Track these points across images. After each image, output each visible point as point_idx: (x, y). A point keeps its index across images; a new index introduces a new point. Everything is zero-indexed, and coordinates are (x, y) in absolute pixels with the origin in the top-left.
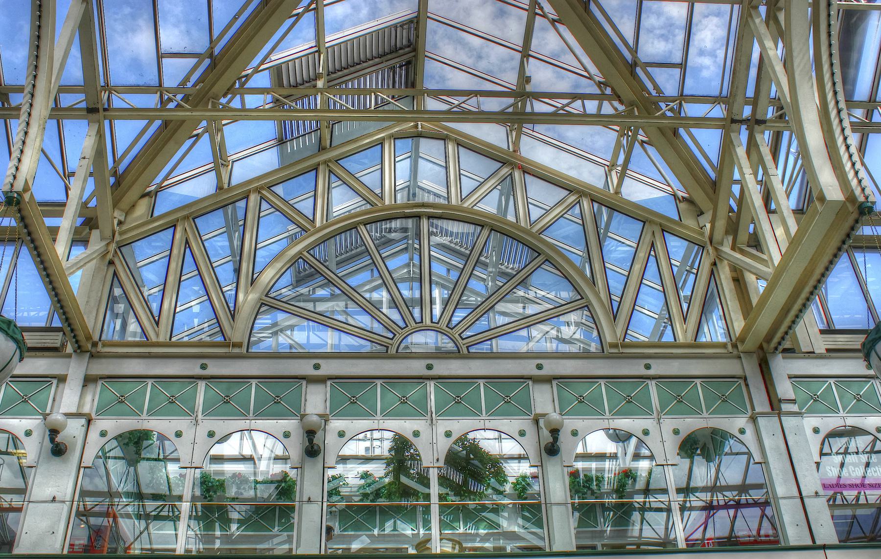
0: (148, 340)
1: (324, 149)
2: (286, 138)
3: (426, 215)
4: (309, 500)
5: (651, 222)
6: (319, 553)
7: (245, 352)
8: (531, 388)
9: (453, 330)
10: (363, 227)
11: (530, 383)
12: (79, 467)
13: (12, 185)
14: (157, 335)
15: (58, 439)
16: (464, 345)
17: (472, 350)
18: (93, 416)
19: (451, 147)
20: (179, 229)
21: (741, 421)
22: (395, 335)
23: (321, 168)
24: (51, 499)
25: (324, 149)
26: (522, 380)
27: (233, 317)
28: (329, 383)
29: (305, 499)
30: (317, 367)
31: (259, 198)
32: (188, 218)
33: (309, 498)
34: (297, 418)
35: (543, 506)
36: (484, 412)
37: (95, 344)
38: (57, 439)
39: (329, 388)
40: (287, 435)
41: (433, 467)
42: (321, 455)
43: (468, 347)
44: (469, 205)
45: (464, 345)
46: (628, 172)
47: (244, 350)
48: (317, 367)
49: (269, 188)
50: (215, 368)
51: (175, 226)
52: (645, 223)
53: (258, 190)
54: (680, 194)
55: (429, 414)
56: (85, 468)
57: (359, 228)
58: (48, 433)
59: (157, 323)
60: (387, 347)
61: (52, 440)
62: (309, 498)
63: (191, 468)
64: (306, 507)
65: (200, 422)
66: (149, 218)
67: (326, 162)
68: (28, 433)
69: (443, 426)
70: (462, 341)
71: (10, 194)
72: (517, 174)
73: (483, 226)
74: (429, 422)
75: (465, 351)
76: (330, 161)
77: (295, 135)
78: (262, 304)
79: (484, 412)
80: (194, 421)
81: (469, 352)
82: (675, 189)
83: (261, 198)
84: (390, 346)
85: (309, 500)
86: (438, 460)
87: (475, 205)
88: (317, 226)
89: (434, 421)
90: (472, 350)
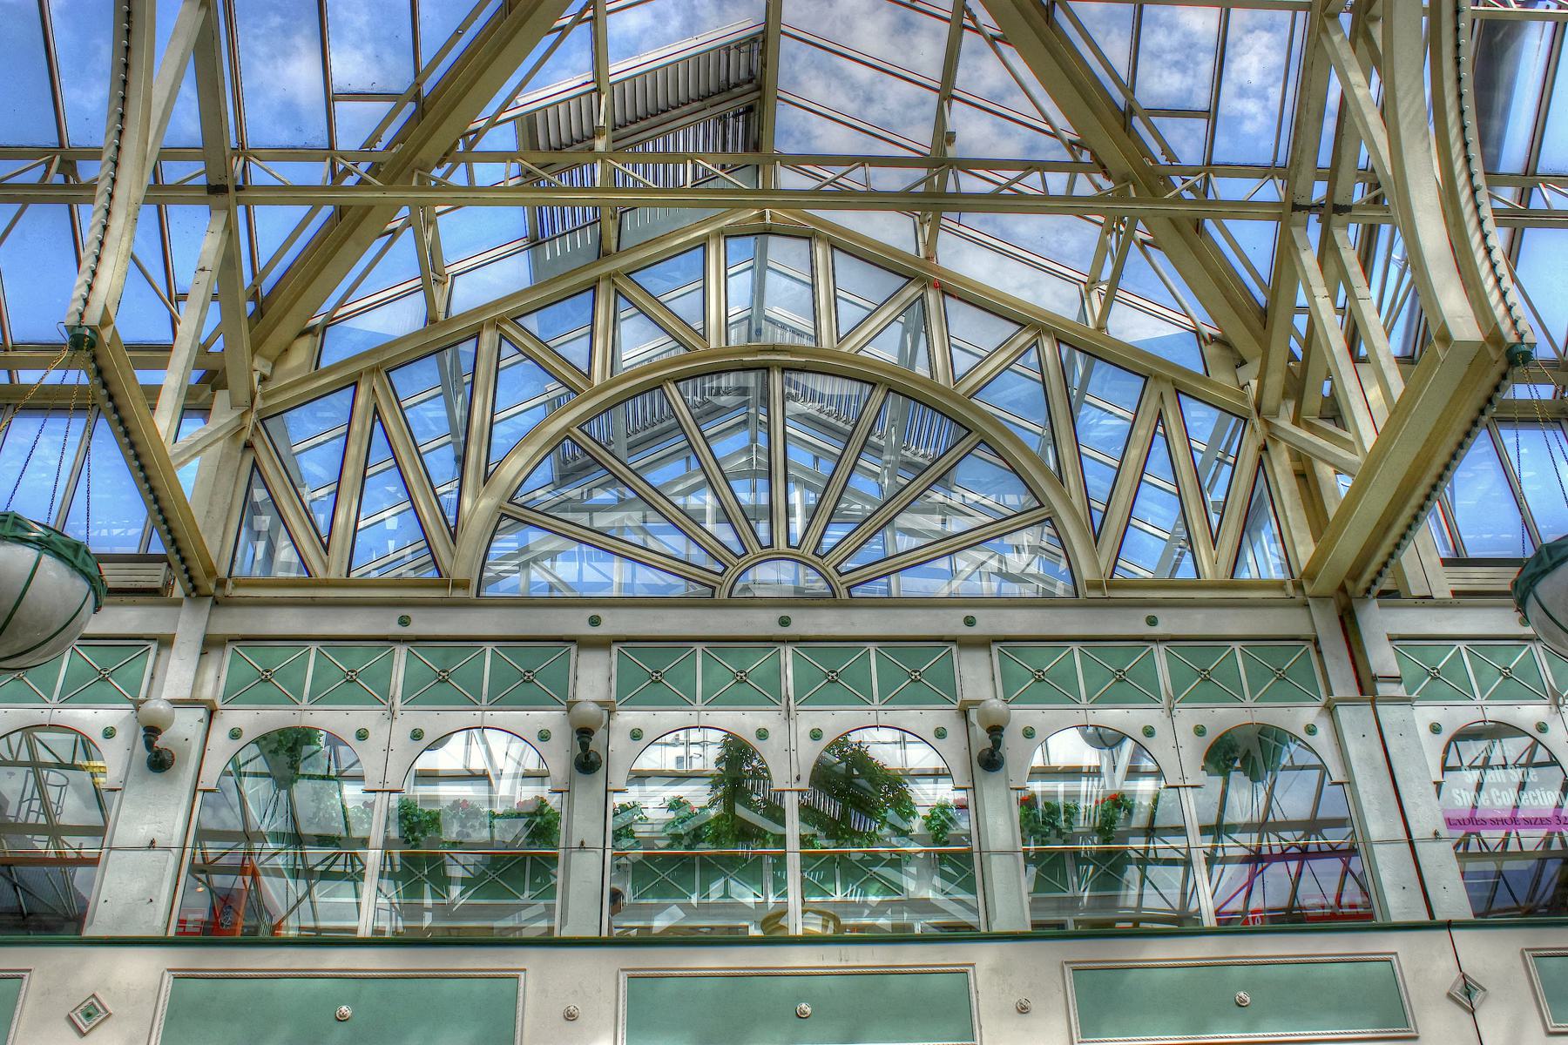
0: (310, 575)
1: (607, 254)
2: (543, 236)
3: (778, 367)
4: (582, 845)
5: (1158, 377)
6: (597, 935)
7: (474, 596)
8: (955, 656)
9: (825, 560)
10: (672, 387)
11: (954, 648)
12: (195, 791)
13: (82, 315)
14: (326, 568)
15: (160, 743)
16: (842, 584)
17: (857, 593)
18: (219, 704)
19: (820, 251)
20: (363, 389)
21: (1309, 713)
22: (726, 568)
23: (602, 286)
24: (148, 844)
25: (607, 254)
26: (940, 644)
27: (454, 537)
28: (615, 648)
29: (575, 843)
30: (595, 621)
31: (497, 337)
32: (378, 370)
33: (582, 843)
34: (561, 707)
35: (976, 856)
36: (876, 698)
37: (221, 584)
38: (157, 743)
39: (615, 658)
40: (544, 736)
41: (383, 791)
42: (602, 770)
43: (849, 589)
44: (852, 349)
45: (842, 584)
46: (1119, 293)
47: (472, 593)
48: (970, 622)
49: (514, 320)
50: (423, 624)
51: (356, 384)
52: (1147, 378)
53: (496, 324)
54: (1207, 330)
55: (784, 700)
56: (204, 791)
57: (665, 388)
58: (142, 733)
59: (326, 548)
60: (714, 588)
61: (149, 745)
62: (582, 843)
63: (383, 791)
64: (576, 857)
65: (398, 714)
66: (313, 370)
67: (610, 277)
68: (109, 733)
69: (807, 720)
70: (839, 578)
71: (78, 331)
72: (932, 297)
73: (874, 385)
74: (784, 714)
75: (845, 595)
76: (617, 274)
77: (559, 230)
78: (503, 515)
79: (876, 698)
80: (388, 713)
81: (850, 596)
82: (1198, 321)
83: (502, 337)
84: (718, 587)
85: (582, 845)
86: (798, 778)
87: (861, 349)
88: (596, 384)
89: (793, 713)
90: (857, 593)
